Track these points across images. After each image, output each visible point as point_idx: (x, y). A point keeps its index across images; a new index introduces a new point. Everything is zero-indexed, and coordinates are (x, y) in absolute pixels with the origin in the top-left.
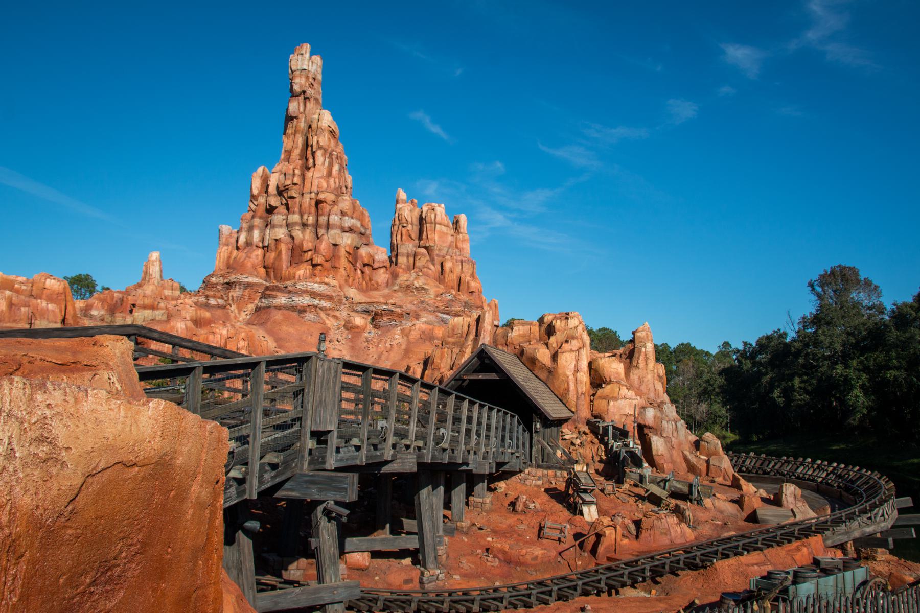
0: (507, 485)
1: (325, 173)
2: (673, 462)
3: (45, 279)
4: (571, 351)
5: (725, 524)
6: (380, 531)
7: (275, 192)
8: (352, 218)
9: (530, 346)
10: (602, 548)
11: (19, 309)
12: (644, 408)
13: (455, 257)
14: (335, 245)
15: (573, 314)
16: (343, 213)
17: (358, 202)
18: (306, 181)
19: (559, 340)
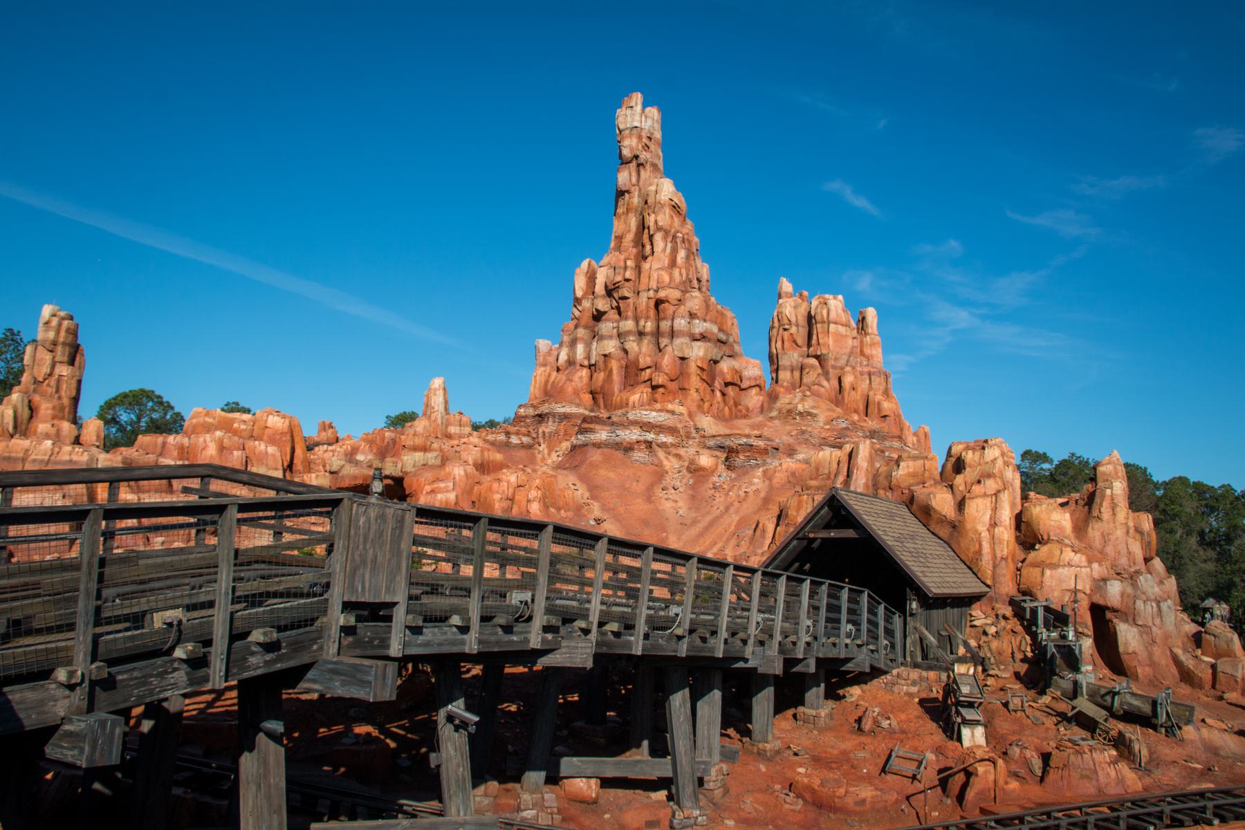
0: (863, 692)
1: (666, 262)
2: (1153, 664)
3: (268, 416)
4: (985, 495)
5: (1210, 769)
6: (634, 750)
7: (603, 292)
8: (705, 321)
9: (925, 490)
10: (972, 794)
11: (231, 453)
12: (1104, 580)
13: (859, 369)
14: (683, 359)
15: (994, 442)
16: (692, 316)
17: (713, 299)
18: (642, 274)
19: (969, 481)
